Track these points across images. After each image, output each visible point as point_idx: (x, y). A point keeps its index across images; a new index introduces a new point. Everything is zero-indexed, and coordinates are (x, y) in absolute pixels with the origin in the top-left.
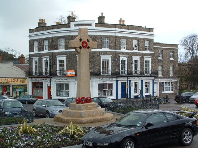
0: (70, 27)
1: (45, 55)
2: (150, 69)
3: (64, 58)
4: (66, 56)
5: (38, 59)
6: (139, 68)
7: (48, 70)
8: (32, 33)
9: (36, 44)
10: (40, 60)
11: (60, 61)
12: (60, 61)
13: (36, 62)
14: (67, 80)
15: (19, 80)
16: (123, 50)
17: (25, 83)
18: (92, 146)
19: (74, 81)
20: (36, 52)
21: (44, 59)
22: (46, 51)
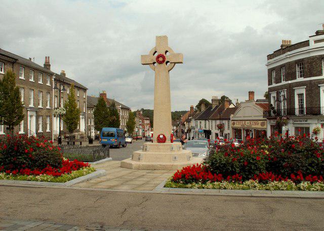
0: (308, 45)
1: (282, 87)
2: (305, 106)
3: (303, 90)
4: (305, 87)
5: (305, 89)
6: (297, 106)
7: (305, 106)
8: (270, 60)
9: (274, 74)
10: (278, 94)
11: (299, 95)
12: (299, 95)
13: (300, 95)
14: (306, 121)
15: (260, 122)
16: (299, 79)
17: (265, 127)
18: (39, 132)
19: (316, 124)
20: (274, 85)
21: (297, 91)
22: (284, 83)
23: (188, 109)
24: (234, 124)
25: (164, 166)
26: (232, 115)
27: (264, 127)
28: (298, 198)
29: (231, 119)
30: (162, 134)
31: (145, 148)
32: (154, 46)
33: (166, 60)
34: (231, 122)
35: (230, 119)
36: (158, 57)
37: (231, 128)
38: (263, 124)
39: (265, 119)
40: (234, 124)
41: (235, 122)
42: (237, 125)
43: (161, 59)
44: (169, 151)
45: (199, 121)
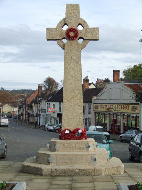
15: (130, 106)
17: (137, 112)
23: (36, 88)
24: (96, 107)
25: (84, 170)
26: (95, 98)
27: (136, 112)
28: (106, 181)
29: (93, 102)
30: (68, 130)
31: (53, 147)
32: (64, 16)
33: (79, 36)
34: (93, 106)
35: (91, 102)
36: (68, 31)
37: (93, 112)
38: (134, 109)
39: (40, 93)
40: (96, 107)
41: (99, 105)
42: (101, 109)
43: (72, 35)
44: (85, 150)
45: (51, 103)
